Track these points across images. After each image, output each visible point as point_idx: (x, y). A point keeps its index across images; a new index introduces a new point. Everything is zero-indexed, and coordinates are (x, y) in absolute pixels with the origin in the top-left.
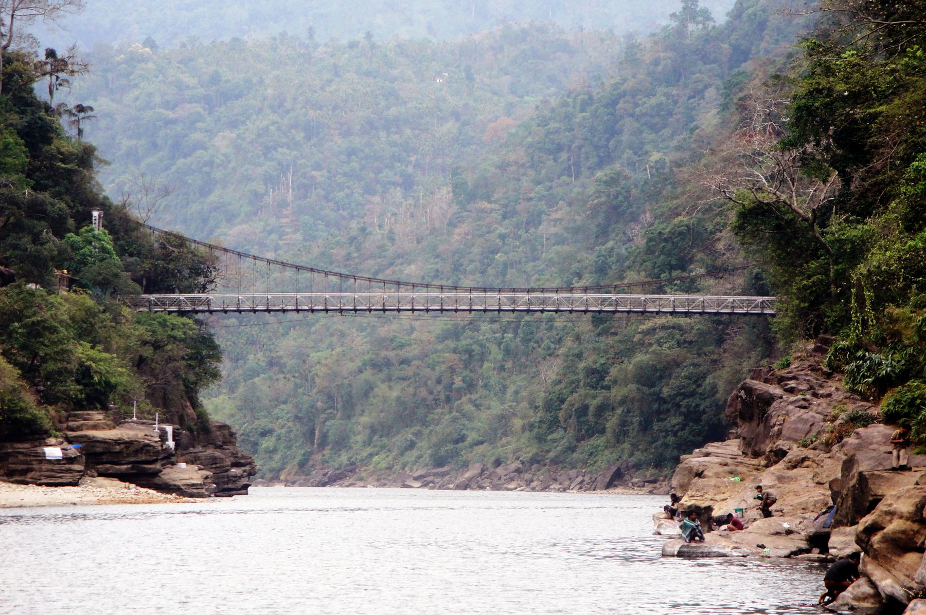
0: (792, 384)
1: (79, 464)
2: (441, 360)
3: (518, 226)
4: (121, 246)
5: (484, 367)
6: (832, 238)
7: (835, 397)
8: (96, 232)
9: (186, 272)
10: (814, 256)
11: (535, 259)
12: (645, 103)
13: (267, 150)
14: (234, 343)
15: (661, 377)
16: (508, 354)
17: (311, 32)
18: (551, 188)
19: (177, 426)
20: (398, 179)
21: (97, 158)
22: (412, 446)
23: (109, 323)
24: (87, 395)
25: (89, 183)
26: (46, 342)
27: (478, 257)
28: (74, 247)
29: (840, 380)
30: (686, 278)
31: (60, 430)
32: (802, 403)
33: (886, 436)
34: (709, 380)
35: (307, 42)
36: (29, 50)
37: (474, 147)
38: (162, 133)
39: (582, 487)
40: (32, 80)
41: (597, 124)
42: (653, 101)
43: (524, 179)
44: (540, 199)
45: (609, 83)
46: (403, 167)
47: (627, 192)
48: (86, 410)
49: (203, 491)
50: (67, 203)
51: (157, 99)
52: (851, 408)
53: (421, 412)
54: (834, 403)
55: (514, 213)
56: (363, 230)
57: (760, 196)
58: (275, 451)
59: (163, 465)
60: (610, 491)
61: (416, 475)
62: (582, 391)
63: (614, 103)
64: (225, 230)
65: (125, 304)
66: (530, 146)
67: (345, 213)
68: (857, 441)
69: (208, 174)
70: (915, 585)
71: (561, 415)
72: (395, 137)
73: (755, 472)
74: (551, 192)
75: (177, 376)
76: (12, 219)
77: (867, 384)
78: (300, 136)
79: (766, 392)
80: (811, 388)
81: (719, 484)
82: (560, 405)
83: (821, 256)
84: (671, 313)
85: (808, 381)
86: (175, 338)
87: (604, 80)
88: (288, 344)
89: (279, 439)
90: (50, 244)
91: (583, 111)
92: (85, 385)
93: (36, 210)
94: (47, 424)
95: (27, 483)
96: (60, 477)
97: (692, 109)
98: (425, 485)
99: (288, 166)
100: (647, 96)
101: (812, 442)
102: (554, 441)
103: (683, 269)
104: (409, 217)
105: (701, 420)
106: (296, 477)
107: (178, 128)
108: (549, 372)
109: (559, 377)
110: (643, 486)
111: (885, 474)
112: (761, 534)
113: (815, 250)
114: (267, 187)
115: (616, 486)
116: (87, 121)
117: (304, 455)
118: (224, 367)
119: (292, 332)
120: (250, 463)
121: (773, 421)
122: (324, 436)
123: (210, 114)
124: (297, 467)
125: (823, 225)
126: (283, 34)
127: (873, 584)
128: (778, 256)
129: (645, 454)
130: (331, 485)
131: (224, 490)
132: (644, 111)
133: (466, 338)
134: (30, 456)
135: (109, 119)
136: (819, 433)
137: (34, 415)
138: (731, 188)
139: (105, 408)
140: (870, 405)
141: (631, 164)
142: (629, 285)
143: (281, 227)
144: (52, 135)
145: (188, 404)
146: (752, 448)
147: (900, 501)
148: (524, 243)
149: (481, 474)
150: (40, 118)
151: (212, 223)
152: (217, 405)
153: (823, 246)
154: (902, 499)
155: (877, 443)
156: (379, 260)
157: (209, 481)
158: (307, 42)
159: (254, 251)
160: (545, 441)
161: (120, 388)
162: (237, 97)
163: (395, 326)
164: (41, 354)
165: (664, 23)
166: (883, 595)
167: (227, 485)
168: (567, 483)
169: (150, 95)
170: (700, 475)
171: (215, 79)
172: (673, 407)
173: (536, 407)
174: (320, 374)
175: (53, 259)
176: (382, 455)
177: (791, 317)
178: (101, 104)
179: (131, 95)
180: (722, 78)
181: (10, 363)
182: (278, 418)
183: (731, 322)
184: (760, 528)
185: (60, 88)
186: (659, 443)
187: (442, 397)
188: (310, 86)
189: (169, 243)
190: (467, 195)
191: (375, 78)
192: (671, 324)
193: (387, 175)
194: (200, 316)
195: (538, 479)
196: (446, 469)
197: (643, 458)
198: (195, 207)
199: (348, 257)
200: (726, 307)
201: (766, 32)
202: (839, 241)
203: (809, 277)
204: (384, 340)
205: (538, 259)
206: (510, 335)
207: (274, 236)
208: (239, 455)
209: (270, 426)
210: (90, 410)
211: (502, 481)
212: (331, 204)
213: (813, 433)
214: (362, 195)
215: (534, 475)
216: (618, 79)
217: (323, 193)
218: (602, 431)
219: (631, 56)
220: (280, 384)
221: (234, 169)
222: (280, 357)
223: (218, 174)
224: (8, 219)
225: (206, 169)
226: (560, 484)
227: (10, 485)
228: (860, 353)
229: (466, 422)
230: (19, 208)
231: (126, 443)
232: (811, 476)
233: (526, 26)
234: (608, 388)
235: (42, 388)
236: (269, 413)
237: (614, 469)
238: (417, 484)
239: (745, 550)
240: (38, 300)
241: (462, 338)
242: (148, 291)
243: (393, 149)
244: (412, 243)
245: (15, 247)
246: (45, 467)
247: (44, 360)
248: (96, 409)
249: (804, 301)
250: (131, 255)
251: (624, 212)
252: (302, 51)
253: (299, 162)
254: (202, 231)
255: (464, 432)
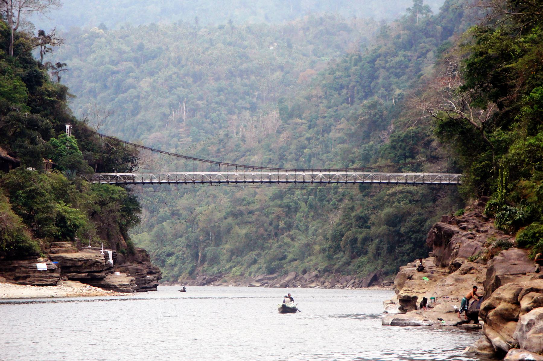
0: (465, 224)
1: (57, 273)
2: (272, 211)
3: (317, 133)
4: (82, 145)
5: (297, 216)
6: (494, 140)
7: (489, 232)
8: (68, 137)
9: (120, 161)
10: (484, 150)
11: (328, 152)
12: (392, 60)
13: (171, 89)
14: (152, 202)
15: (400, 222)
16: (311, 208)
17: (197, 20)
18: (337, 110)
19: (115, 251)
20: (248, 105)
21: (68, 94)
22: (255, 262)
23: (75, 190)
24: (62, 232)
25: (64, 108)
26: (38, 202)
27: (294, 151)
28: (55, 146)
29: (493, 222)
30: (415, 163)
31: (46, 253)
32: (470, 236)
33: (518, 255)
34: (428, 223)
35: (194, 26)
36: (29, 31)
37: (292, 86)
38: (109, 79)
39: (354, 286)
40: (30, 49)
41: (365, 74)
42: (397, 59)
43: (321, 105)
44: (331, 117)
45: (370, 48)
46: (251, 98)
47: (381, 113)
48: (61, 241)
49: (130, 288)
50: (50, 120)
51: (107, 59)
52: (499, 238)
53: (260, 242)
54: (489, 236)
55: (315, 125)
56: (227, 135)
57: (452, 115)
58: (175, 265)
59: (106, 274)
60: (370, 288)
61: (258, 279)
62: (354, 230)
63: (373, 61)
64: (146, 136)
65: (84, 179)
66: (325, 86)
67: (216, 126)
68: (501, 258)
69: (137, 102)
70: (513, 341)
71: (342, 243)
72: (246, 81)
73: (443, 276)
74: (337, 112)
75: (115, 221)
76: (18, 130)
77: (509, 224)
78: (190, 80)
79: (449, 229)
80: (476, 227)
81: (421, 283)
82: (341, 238)
83: (488, 150)
84: (405, 184)
85: (474, 223)
86: (114, 199)
87: (368, 47)
88: (183, 202)
89: (177, 258)
90: (41, 144)
91: (356, 65)
92: (61, 227)
93: (32, 125)
94: (38, 250)
95: (26, 284)
96: (46, 281)
97: (420, 64)
98: (262, 285)
99: (183, 98)
100: (393, 57)
101: (476, 259)
102: (338, 258)
103: (413, 157)
104: (255, 127)
105: (423, 247)
106: (188, 281)
107: (119, 76)
108: (334, 219)
109: (341, 221)
110: (390, 285)
111: (511, 277)
112: (440, 313)
113: (484, 146)
114: (171, 110)
115: (374, 285)
116: (62, 72)
117: (192, 267)
118: (144, 215)
119: (185, 195)
120: (158, 272)
121: (453, 246)
122: (204, 257)
123: (138, 68)
124: (188, 275)
125: (490, 132)
126: (180, 21)
127: (489, 340)
128: (463, 149)
129: (391, 266)
130: (208, 285)
131: (143, 288)
132: (391, 65)
133: (287, 198)
134: (28, 268)
135: (79, 71)
136: (480, 253)
137: (31, 244)
138: (435, 110)
139: (72, 240)
140: (509, 237)
141: (384, 97)
142: (380, 167)
143: (179, 134)
144: (43, 81)
145: (122, 237)
146: (441, 262)
147: (505, 292)
148: (321, 143)
149: (295, 278)
150: (35, 71)
151: (139, 131)
152: (140, 238)
153: (488, 144)
154: (506, 291)
155: (513, 259)
156: (236, 153)
157: (133, 283)
158: (194, 26)
159: (163, 148)
160: (332, 259)
161: (81, 228)
162: (154, 58)
163: (246, 191)
164: (35, 208)
165: (403, 13)
166: (495, 347)
167: (144, 285)
168: (345, 284)
169: (103, 57)
170: (410, 278)
171: (141, 47)
172: (407, 239)
173: (327, 239)
174: (202, 219)
175: (42, 153)
176: (238, 268)
177: (470, 185)
178: (72, 63)
179: (92, 57)
180: (437, 46)
181: (16, 214)
182: (177, 246)
183: (440, 188)
184: (440, 309)
185: (46, 53)
186: (399, 260)
187: (273, 233)
188: (196, 51)
189: (110, 143)
190: (288, 115)
191: (234, 46)
192: (405, 190)
193: (241, 103)
194: (129, 186)
195: (328, 281)
196: (275, 275)
197: (389, 269)
198: (129, 123)
199: (218, 151)
200: (437, 180)
201: (463, 19)
202: (498, 141)
203: (481, 162)
204: (238, 200)
205: (330, 152)
206: (313, 197)
207: (175, 139)
208: (152, 268)
209: (172, 250)
210: (64, 241)
211: (307, 282)
212: (208, 120)
213: (477, 253)
214: (227, 115)
215: (326, 279)
216: (376, 47)
217: (203, 114)
218: (366, 253)
219: (384, 33)
220: (178, 226)
221: (152, 100)
222: (178, 210)
223: (142, 103)
224: (16, 130)
225: (135, 100)
226: (341, 284)
227: (16, 285)
228: (504, 206)
229: (286, 247)
230: (23, 123)
231: (84, 260)
232: (475, 278)
233: (322, 16)
234: (369, 228)
235: (35, 229)
236: (172, 243)
237: (372, 275)
238: (258, 284)
239: (431, 321)
240: (33, 177)
241: (285, 198)
242: (98, 171)
243: (245, 88)
244: (256, 143)
245: (20, 146)
246: (37, 275)
247: (36, 212)
248: (67, 240)
249: (477, 176)
250: (89, 150)
251: (379, 124)
252: (192, 31)
253: (190, 96)
254: (133, 136)
255: (286, 253)
